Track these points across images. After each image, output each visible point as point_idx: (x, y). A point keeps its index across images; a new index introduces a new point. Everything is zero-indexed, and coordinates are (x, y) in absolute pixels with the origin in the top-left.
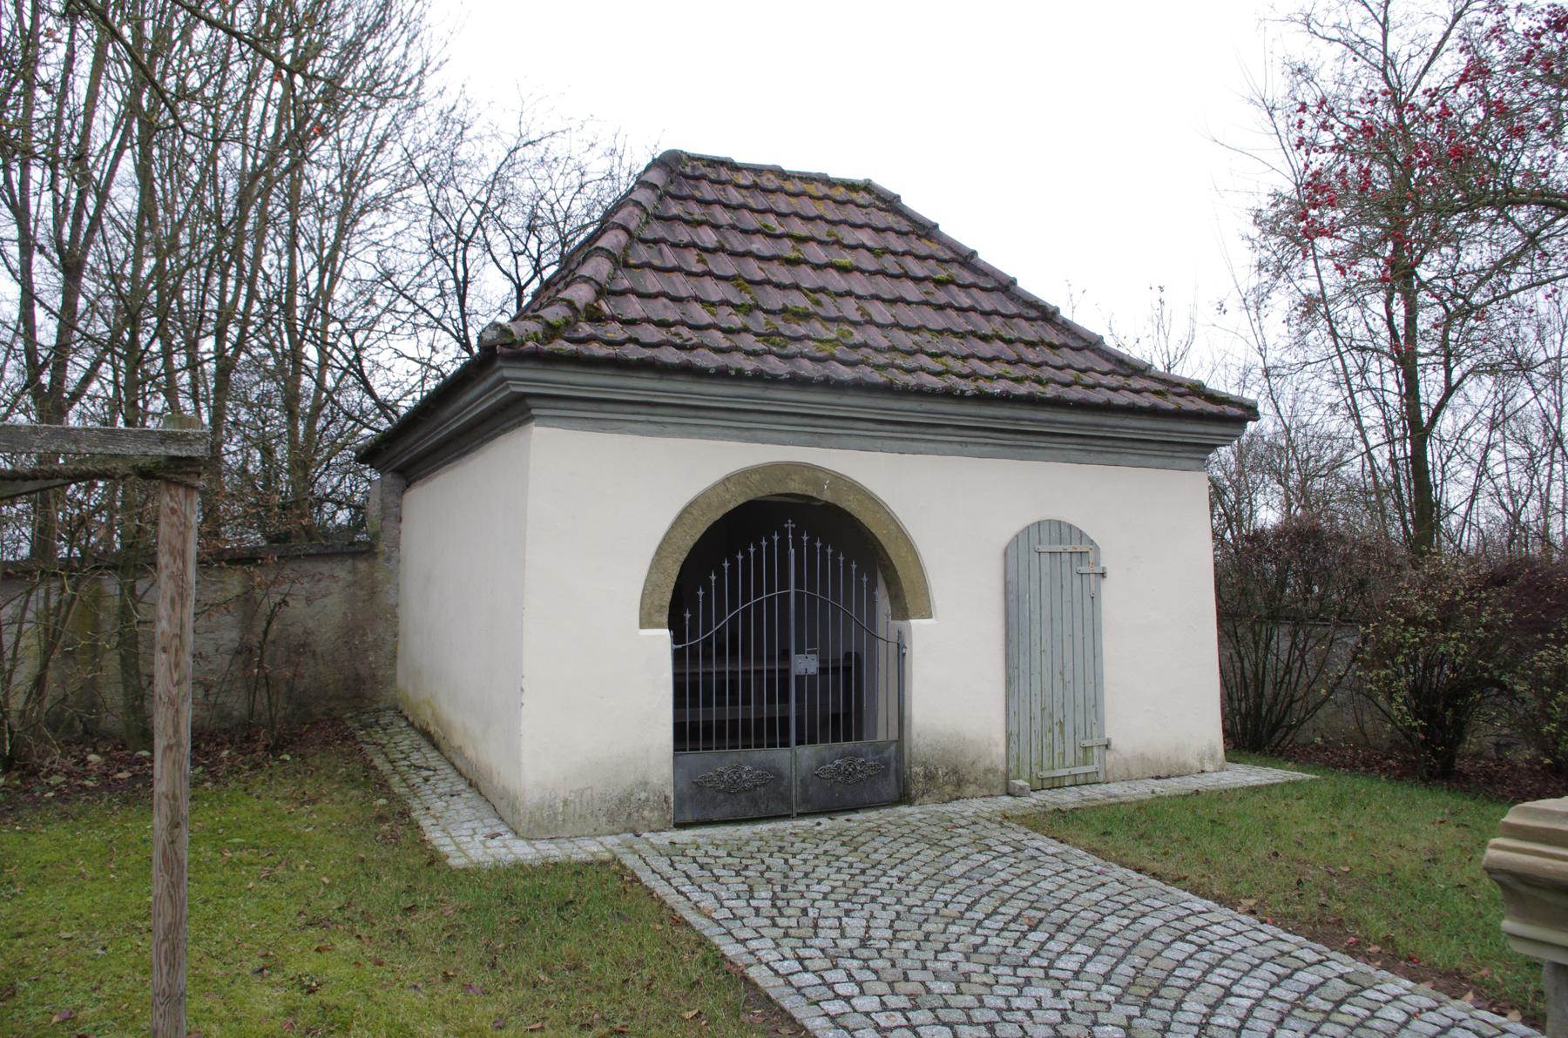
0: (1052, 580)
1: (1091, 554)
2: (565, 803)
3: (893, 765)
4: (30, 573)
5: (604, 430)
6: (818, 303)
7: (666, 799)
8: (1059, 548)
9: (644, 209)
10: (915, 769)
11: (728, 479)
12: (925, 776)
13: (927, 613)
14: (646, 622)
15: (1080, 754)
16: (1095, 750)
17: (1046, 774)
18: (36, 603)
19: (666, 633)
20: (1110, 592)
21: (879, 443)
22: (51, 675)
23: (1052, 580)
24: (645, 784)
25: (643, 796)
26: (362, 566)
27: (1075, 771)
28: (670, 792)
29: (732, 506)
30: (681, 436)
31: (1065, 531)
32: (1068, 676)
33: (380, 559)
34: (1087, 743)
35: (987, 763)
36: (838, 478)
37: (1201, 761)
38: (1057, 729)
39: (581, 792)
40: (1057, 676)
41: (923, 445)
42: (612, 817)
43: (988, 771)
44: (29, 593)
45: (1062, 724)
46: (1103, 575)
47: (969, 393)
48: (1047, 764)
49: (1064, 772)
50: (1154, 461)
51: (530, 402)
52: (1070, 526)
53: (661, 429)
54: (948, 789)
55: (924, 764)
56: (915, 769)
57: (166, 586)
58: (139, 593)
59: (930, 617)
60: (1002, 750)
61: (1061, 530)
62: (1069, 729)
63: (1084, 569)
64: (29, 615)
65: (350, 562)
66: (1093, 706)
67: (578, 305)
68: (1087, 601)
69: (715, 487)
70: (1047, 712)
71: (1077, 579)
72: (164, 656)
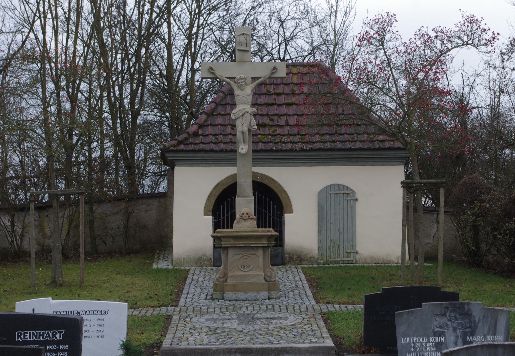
0: (337, 204)
1: (351, 194)
2: (184, 258)
3: (280, 254)
4: (65, 205)
5: (194, 166)
6: (272, 120)
7: (211, 259)
8: (339, 192)
9: (224, 93)
10: (286, 255)
11: (228, 177)
12: (289, 258)
13: (291, 212)
14: (205, 214)
15: (346, 255)
16: (352, 254)
17: (332, 260)
18: (67, 213)
19: (211, 217)
20: (360, 208)
21: (275, 165)
22: (71, 232)
23: (337, 204)
24: (205, 255)
25: (205, 258)
26: (162, 200)
27: (343, 259)
28: (212, 257)
29: (230, 184)
30: (215, 166)
31: (341, 187)
32: (341, 231)
33: (168, 198)
34: (348, 251)
35: (311, 255)
36: (262, 175)
37: (398, 260)
38: (337, 247)
39: (188, 256)
40: (337, 231)
41: (290, 164)
42: (196, 263)
43: (311, 258)
44: (65, 210)
45: (339, 246)
46: (356, 200)
47: (298, 150)
48: (332, 256)
49: (340, 259)
50: (380, 163)
51: (174, 161)
52: (343, 185)
53: (210, 165)
54: (297, 262)
55: (289, 254)
56: (286, 255)
57: (81, 206)
58: (94, 209)
59: (292, 213)
60: (316, 252)
61: (339, 187)
62: (341, 247)
63: (348, 199)
64: (65, 216)
65: (158, 199)
66: (352, 240)
67: (190, 133)
68: (350, 209)
69: (225, 179)
70: (333, 241)
71: (345, 202)
72: (138, 303)
